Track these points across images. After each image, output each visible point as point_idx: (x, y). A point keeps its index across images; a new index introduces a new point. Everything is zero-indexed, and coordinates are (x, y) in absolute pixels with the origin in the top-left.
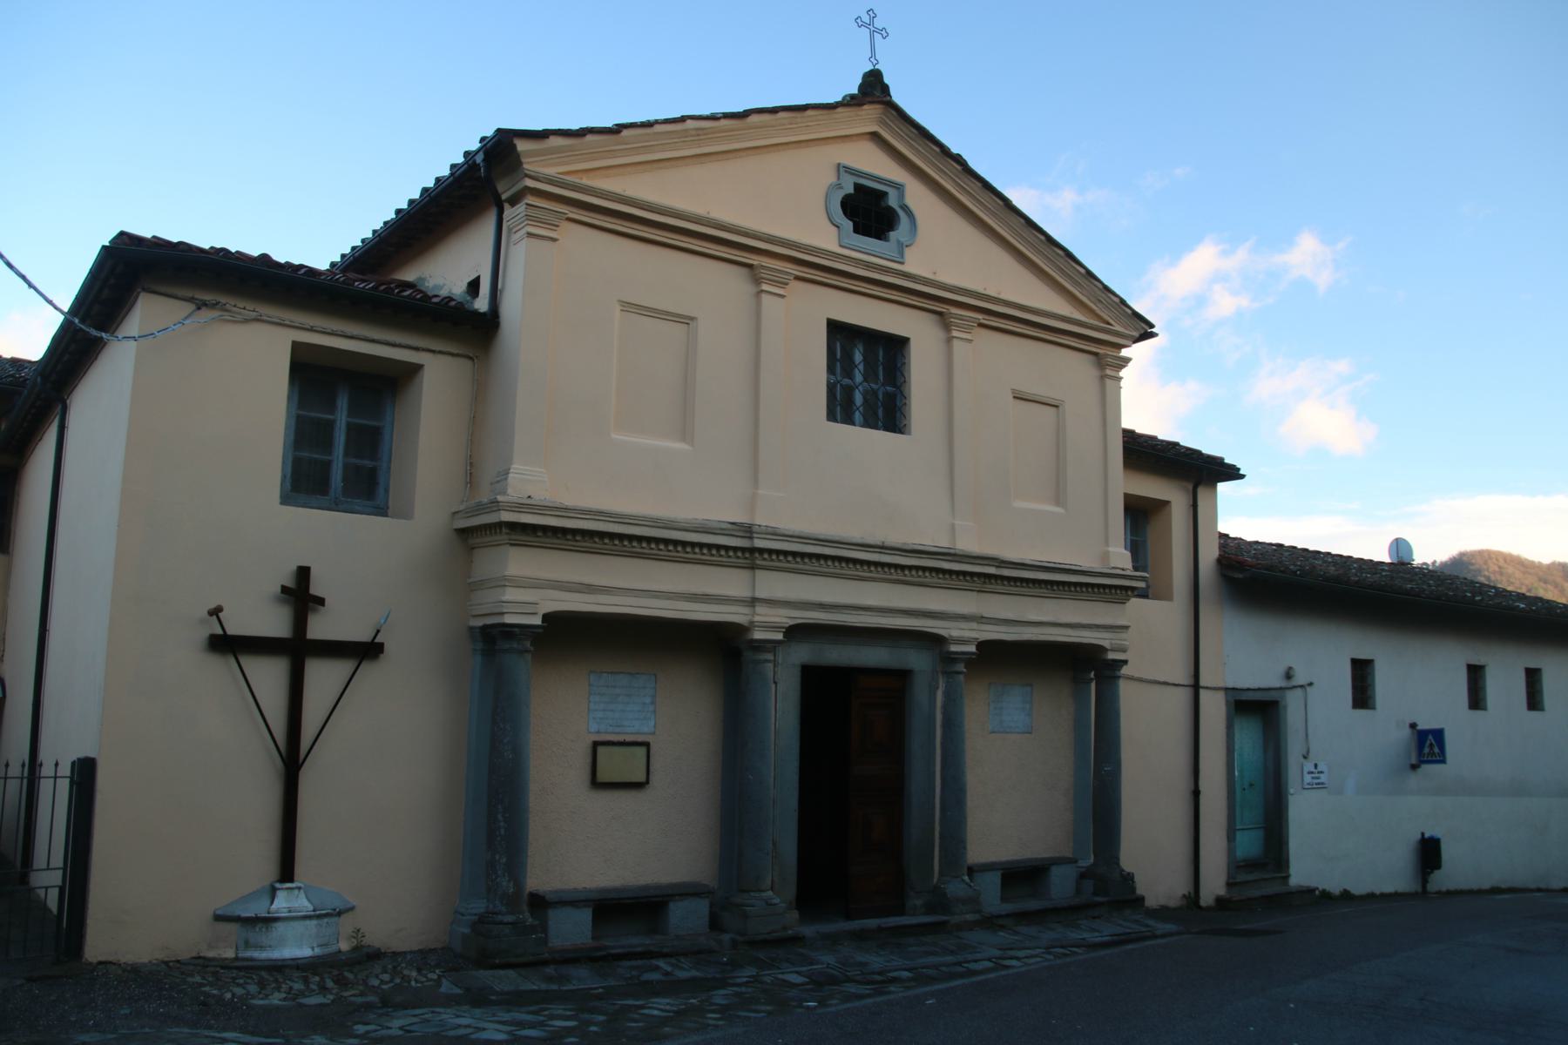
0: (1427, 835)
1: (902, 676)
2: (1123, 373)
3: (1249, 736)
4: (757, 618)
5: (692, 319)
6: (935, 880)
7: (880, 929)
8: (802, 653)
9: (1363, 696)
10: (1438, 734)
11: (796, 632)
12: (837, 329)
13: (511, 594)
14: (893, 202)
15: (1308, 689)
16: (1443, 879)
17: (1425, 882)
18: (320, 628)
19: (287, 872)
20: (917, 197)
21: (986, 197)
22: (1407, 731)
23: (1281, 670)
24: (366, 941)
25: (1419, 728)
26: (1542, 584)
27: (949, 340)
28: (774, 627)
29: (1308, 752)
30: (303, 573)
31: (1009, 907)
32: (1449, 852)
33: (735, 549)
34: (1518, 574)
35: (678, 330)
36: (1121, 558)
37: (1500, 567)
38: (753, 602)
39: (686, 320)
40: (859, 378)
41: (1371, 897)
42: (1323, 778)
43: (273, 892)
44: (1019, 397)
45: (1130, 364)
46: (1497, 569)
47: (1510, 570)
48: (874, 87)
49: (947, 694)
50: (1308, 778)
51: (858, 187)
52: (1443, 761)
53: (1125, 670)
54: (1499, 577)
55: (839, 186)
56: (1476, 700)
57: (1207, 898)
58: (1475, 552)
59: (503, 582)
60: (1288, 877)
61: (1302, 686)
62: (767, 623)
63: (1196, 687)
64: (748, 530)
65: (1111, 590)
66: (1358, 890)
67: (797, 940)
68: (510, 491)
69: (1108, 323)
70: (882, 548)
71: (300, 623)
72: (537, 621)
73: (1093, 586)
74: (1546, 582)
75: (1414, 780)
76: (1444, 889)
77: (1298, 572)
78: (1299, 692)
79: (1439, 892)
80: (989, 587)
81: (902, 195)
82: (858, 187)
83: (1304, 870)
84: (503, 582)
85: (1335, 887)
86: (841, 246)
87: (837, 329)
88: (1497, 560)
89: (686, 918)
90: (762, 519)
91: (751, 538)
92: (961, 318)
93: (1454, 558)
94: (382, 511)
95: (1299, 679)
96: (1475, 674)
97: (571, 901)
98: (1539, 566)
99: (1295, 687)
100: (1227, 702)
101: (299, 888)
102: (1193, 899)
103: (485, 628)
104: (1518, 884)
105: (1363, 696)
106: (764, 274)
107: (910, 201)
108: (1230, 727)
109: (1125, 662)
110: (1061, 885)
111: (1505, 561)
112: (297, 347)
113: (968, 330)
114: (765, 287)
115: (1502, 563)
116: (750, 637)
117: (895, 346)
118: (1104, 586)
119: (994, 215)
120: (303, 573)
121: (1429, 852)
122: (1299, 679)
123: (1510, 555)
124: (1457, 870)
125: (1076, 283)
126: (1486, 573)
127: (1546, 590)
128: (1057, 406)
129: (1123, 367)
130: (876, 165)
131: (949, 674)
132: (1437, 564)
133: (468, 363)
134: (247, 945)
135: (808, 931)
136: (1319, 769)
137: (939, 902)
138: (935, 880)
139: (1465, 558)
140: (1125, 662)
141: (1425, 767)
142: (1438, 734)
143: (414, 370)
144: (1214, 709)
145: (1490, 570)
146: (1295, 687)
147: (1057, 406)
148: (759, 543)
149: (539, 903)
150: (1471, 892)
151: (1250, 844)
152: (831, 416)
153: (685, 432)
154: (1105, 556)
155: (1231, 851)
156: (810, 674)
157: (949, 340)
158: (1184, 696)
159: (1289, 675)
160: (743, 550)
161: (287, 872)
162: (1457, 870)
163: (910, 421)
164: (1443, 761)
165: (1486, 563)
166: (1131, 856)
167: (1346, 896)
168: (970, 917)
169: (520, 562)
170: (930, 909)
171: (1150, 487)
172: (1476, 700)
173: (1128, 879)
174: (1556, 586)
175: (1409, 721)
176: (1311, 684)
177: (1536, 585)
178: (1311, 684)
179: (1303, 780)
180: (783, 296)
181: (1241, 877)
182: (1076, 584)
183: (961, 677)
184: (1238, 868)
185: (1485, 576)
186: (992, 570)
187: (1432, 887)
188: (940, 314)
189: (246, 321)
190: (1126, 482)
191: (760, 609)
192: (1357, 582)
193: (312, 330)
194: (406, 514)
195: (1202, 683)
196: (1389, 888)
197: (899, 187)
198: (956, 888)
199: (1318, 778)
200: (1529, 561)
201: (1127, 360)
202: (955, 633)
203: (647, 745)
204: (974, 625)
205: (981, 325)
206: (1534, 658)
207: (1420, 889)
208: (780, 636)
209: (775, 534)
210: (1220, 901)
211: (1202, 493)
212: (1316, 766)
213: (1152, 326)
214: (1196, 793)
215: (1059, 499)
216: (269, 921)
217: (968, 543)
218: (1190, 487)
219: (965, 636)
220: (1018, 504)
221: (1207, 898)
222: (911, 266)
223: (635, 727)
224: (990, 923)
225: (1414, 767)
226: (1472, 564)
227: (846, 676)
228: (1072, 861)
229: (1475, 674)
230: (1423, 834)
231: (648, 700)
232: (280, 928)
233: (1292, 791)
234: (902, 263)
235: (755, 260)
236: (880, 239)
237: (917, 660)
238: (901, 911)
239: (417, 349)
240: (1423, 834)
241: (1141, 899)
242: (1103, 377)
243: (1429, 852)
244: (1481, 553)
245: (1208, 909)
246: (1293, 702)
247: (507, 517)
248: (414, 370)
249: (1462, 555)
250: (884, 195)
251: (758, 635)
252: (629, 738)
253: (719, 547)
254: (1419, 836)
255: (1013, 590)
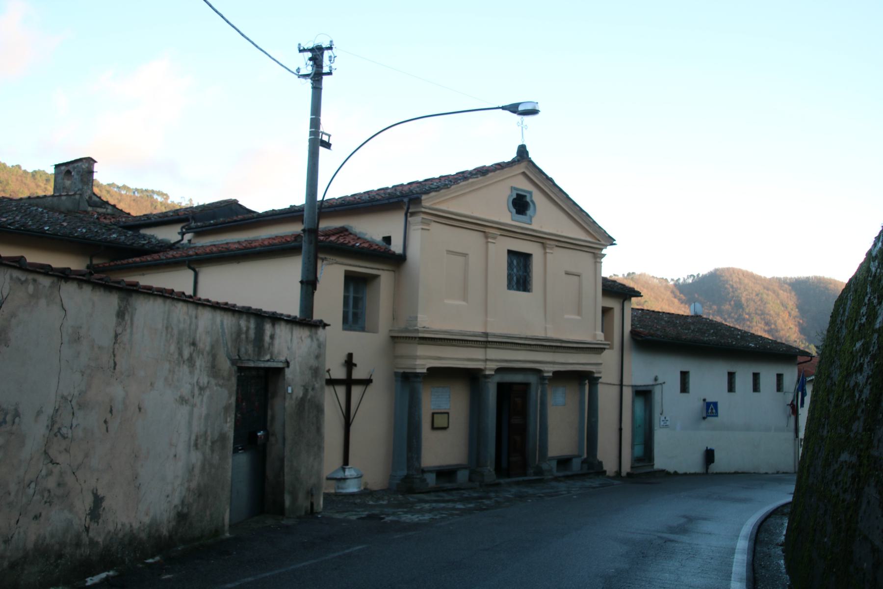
0: (709, 448)
1: (527, 385)
2: (602, 260)
3: (640, 405)
4: (487, 366)
5: (467, 254)
6: (537, 463)
7: (523, 480)
8: (498, 378)
9: (684, 388)
10: (715, 404)
11: (499, 370)
12: (510, 253)
13: (419, 362)
14: (528, 199)
15: (663, 385)
16: (715, 467)
17: (707, 468)
18: (357, 374)
19: (346, 462)
20: (537, 198)
21: (556, 190)
22: (702, 402)
23: (653, 377)
24: (369, 487)
25: (707, 401)
26: (765, 291)
27: (545, 253)
28: (491, 369)
29: (662, 412)
30: (350, 356)
31: (561, 474)
32: (717, 456)
33: (482, 342)
34: (751, 284)
35: (461, 259)
36: (600, 336)
37: (740, 279)
38: (486, 360)
39: (465, 255)
40: (515, 270)
41: (685, 474)
42: (668, 423)
43: (344, 470)
44: (567, 273)
45: (606, 256)
46: (738, 280)
47: (746, 281)
48: (522, 152)
49: (542, 392)
50: (662, 423)
51: (517, 195)
52: (717, 416)
53: (600, 380)
54: (739, 286)
55: (512, 196)
56: (731, 388)
57: (624, 473)
58: (725, 269)
59: (415, 358)
60: (653, 465)
61: (661, 384)
62: (490, 368)
63: (621, 385)
64: (486, 334)
65: (598, 350)
66: (681, 471)
67: (498, 484)
68: (419, 325)
69: (599, 241)
70: (526, 338)
71: (349, 373)
72: (425, 371)
73: (591, 348)
74: (768, 289)
75: (704, 424)
76: (715, 472)
77: (662, 337)
78: (659, 386)
79: (713, 473)
80: (557, 350)
81: (531, 197)
82: (517, 195)
83: (660, 462)
84: (415, 358)
85: (671, 469)
86: (513, 220)
87: (510, 253)
88: (738, 274)
89: (462, 476)
90: (490, 330)
91: (487, 337)
92: (550, 245)
93: (711, 272)
94: (363, 329)
95: (660, 381)
96: (731, 376)
97: (430, 471)
98: (765, 279)
99: (658, 384)
100: (633, 392)
101: (351, 468)
102: (619, 473)
103: (404, 373)
104: (745, 470)
105: (684, 388)
106: (490, 235)
107: (534, 199)
108: (633, 402)
109: (600, 378)
110: (576, 465)
111: (743, 275)
112: (346, 272)
113: (551, 249)
114: (490, 240)
115: (741, 276)
116: (484, 373)
117: (525, 258)
118: (595, 348)
119: (561, 200)
120: (350, 356)
121: (709, 456)
122: (660, 381)
123: (747, 272)
124: (721, 464)
125: (589, 225)
126: (731, 283)
127: (768, 295)
128: (579, 276)
129: (602, 258)
130: (524, 185)
131: (543, 384)
132: (700, 276)
133: (393, 273)
134: (338, 488)
135: (502, 481)
136: (667, 419)
137: (539, 471)
138: (537, 463)
139: (718, 272)
140: (600, 378)
141: (709, 419)
142: (715, 404)
143: (375, 277)
144: (628, 393)
145: (734, 281)
146: (658, 384)
147: (579, 276)
148: (490, 339)
149: (423, 471)
150: (726, 473)
151: (639, 451)
152: (510, 287)
153: (465, 298)
154: (595, 336)
155: (633, 453)
156: (501, 386)
157: (545, 253)
158: (617, 389)
159: (656, 379)
160: (484, 342)
161: (346, 462)
162: (721, 464)
163: (532, 286)
164: (717, 416)
165: (731, 276)
166: (601, 456)
167: (676, 473)
168: (550, 477)
169: (422, 350)
170: (536, 474)
171: (610, 303)
172: (731, 388)
173: (600, 463)
174: (774, 292)
175: (702, 398)
176: (664, 383)
177: (761, 291)
178: (664, 383)
179: (660, 424)
180: (494, 243)
181: (636, 465)
182: (587, 348)
183: (547, 386)
184: (636, 460)
185: (730, 284)
186: (559, 344)
187: (710, 471)
188: (542, 243)
189: (332, 264)
190: (603, 301)
191: (488, 363)
192: (685, 339)
193: (350, 265)
194: (374, 331)
195: (624, 383)
196: (692, 471)
197: (530, 193)
198: (545, 466)
199: (666, 423)
200: (758, 276)
201: (604, 255)
202: (546, 369)
203: (448, 413)
204: (552, 365)
205: (557, 246)
206: (756, 368)
207: (705, 472)
208: (493, 373)
209: (495, 335)
210: (628, 474)
211: (626, 303)
212: (665, 418)
213: (615, 240)
214: (620, 430)
215: (579, 313)
216: (345, 479)
217: (551, 335)
218: (622, 301)
219: (549, 370)
220: (566, 316)
221: (624, 473)
222: (535, 226)
223: (444, 406)
224: (556, 479)
225: (704, 418)
226: (723, 277)
227: (510, 385)
228: (579, 456)
229: (731, 376)
230: (707, 448)
231: (448, 397)
232: (348, 481)
233: (656, 428)
234: (530, 224)
235: (487, 230)
236: (522, 214)
237: (532, 379)
238: (526, 475)
239: (378, 269)
240: (707, 448)
241: (605, 472)
242: (596, 262)
243: (709, 456)
244: (728, 269)
245: (624, 477)
246: (657, 391)
247: (421, 335)
248: (375, 277)
249: (716, 270)
250: (525, 196)
251: (487, 373)
252: (443, 411)
253: (477, 341)
254: (705, 449)
255: (565, 351)
